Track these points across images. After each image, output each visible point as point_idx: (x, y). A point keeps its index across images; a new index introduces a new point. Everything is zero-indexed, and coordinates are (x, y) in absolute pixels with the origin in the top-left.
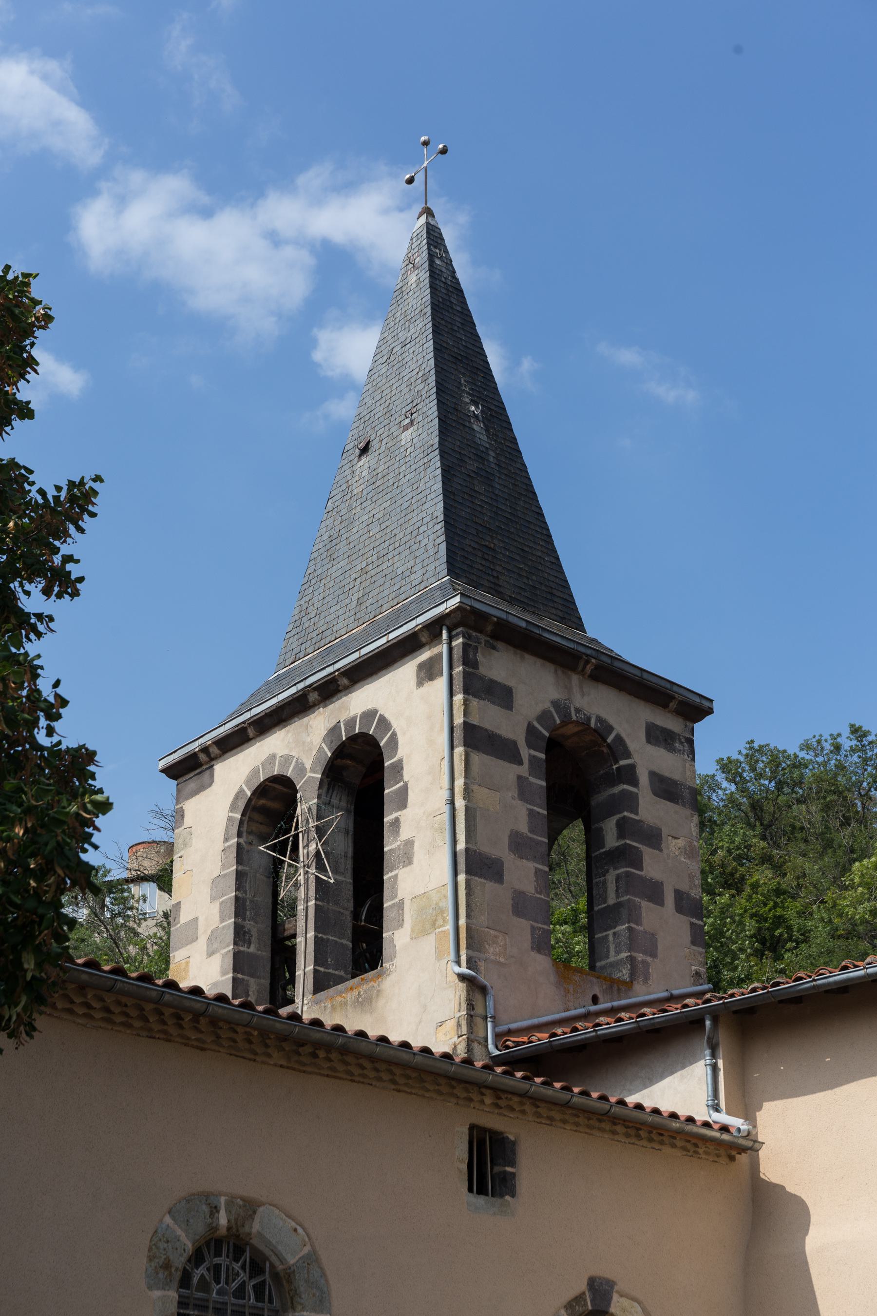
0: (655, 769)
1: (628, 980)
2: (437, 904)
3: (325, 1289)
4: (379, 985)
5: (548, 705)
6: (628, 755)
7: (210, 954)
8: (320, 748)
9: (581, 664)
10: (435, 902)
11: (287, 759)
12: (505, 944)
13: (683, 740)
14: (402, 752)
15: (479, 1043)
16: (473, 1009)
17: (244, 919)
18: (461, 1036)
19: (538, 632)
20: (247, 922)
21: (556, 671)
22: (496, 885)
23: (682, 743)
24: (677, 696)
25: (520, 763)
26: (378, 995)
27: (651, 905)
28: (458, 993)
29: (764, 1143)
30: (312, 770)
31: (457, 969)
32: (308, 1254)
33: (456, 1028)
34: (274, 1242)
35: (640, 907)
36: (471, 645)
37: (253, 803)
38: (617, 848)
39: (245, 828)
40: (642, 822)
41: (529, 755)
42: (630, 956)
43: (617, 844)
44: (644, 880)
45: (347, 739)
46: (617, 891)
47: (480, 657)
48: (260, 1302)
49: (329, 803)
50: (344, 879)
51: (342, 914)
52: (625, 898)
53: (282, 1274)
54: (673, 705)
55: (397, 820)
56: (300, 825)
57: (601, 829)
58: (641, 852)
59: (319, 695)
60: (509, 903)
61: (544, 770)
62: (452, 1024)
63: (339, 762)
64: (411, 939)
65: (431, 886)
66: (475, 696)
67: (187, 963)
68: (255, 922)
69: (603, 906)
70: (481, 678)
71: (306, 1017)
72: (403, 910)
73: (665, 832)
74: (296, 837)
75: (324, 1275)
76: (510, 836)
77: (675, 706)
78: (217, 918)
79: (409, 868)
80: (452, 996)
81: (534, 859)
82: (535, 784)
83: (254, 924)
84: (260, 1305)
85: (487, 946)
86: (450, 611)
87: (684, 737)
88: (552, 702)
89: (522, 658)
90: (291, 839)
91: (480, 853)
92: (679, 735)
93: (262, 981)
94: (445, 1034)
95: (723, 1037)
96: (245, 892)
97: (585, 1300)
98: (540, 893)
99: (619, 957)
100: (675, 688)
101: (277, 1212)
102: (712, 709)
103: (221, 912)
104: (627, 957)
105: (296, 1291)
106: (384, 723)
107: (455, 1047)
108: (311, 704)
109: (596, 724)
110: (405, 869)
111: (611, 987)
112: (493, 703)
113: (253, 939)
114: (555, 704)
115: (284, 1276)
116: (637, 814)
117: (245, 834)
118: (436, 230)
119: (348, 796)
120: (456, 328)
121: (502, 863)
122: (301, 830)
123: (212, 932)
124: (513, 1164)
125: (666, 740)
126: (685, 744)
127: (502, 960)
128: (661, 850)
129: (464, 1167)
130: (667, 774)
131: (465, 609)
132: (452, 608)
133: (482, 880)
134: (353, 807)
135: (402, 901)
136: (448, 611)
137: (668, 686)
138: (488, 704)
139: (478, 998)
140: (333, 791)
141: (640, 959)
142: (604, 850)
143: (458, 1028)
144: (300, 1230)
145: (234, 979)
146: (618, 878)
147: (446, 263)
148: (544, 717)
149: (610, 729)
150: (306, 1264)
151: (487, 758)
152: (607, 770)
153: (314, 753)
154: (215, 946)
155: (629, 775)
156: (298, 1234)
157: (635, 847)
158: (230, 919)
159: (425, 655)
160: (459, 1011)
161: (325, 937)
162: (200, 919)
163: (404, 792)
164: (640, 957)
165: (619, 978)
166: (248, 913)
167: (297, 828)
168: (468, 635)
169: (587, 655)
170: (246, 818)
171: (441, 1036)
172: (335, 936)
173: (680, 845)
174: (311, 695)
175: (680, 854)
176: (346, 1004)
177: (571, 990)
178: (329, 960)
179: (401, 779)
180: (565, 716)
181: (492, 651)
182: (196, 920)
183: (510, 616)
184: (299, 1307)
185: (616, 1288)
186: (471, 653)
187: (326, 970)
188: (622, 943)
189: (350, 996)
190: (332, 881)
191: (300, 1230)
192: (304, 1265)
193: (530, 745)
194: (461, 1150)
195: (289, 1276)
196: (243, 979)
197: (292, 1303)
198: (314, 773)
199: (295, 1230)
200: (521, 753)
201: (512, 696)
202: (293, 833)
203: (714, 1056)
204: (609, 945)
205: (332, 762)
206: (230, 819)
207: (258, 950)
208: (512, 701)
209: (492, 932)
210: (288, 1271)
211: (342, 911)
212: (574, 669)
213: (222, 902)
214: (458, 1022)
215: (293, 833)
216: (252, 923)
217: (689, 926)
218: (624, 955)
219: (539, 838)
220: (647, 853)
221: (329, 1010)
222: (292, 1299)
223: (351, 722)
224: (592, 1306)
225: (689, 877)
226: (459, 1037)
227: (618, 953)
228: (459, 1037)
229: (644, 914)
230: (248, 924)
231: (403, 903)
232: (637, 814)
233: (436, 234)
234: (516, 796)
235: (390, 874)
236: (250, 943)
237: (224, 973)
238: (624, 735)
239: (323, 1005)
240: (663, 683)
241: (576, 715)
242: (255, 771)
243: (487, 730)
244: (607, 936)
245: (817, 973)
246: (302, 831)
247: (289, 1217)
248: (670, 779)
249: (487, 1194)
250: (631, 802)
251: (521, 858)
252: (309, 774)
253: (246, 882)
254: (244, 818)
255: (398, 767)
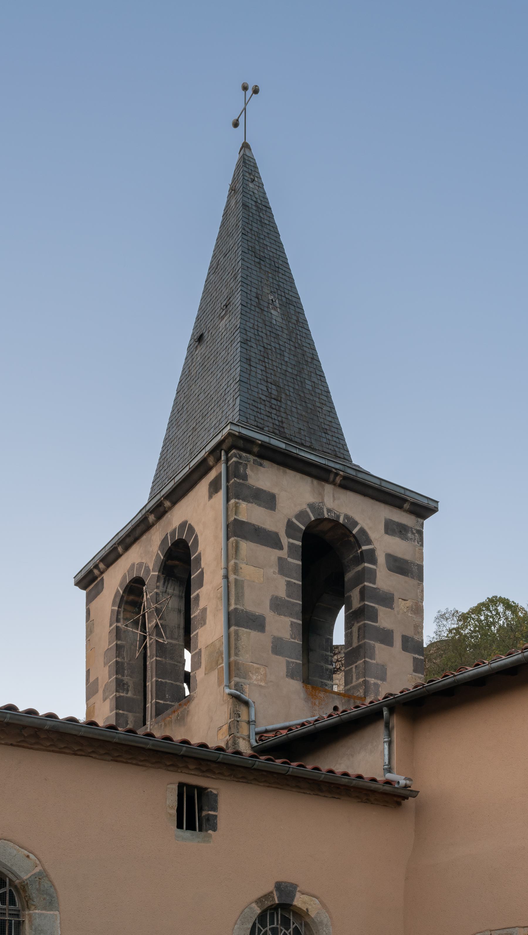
0: (390, 551)
1: (363, 696)
2: (219, 649)
3: (55, 895)
4: (188, 707)
5: (304, 507)
6: (369, 541)
7: (104, 700)
8: (158, 554)
9: (332, 477)
10: (217, 648)
11: (141, 565)
12: (265, 673)
13: (414, 532)
14: (201, 548)
15: (244, 739)
16: (239, 717)
17: (123, 676)
18: (231, 735)
19: (295, 452)
20: (125, 677)
21: (312, 482)
22: (259, 634)
23: (413, 533)
24: (409, 499)
25: (281, 548)
26: (187, 714)
27: (383, 646)
28: (229, 707)
29: (419, 792)
30: (154, 570)
31: (227, 691)
32: (39, 872)
33: (228, 730)
34: (9, 865)
35: (374, 647)
36: (242, 463)
37: (125, 598)
38: (360, 608)
39: (121, 616)
40: (379, 589)
41: (289, 543)
42: (364, 680)
43: (359, 606)
44: (378, 629)
45: (172, 545)
46: (358, 637)
47: (249, 471)
48: (3, 905)
49: (166, 592)
50: (177, 643)
51: (177, 665)
52: (363, 642)
53: (19, 887)
54: (406, 506)
55: (198, 595)
56: (146, 608)
57: (350, 596)
58: (377, 610)
59: (155, 517)
60: (269, 646)
61: (300, 553)
62: (226, 728)
63: (170, 562)
64: (205, 674)
65: (215, 638)
66: (244, 500)
67: (94, 707)
68: (131, 677)
69: (350, 648)
70: (249, 487)
71: (158, 734)
72: (201, 656)
73: (396, 597)
74: (144, 615)
75: (53, 885)
76: (271, 600)
77: (408, 507)
78: (107, 676)
79: (204, 627)
80: (226, 710)
81: (291, 615)
82: (293, 563)
83: (131, 679)
84: (4, 907)
85: (251, 675)
86: (224, 437)
87: (415, 529)
88: (308, 505)
89: (285, 472)
90: (141, 617)
91: (246, 612)
92: (411, 528)
93: (138, 715)
94: (222, 734)
95: (395, 721)
96: (124, 658)
97: (273, 897)
98: (294, 639)
99: (358, 682)
100: (408, 493)
101: (12, 844)
102: (437, 508)
103: (109, 671)
104: (363, 681)
105: (30, 897)
106: (191, 529)
107: (228, 742)
108: (151, 524)
109: (344, 520)
110: (202, 628)
111: (349, 701)
112: (260, 505)
113: (130, 688)
114: (311, 506)
115: (21, 887)
116: (374, 583)
117: (122, 620)
118: (251, 160)
119: (180, 586)
120: (262, 237)
121: (264, 619)
122: (146, 611)
123: (105, 685)
124: (215, 809)
125: (400, 531)
126: (416, 534)
127: (263, 684)
128: (392, 609)
129: (174, 812)
130: (400, 555)
131: (234, 435)
132: (225, 435)
133: (248, 630)
134: (184, 594)
135: (200, 650)
136: (223, 437)
137: (402, 491)
138: (255, 506)
139: (243, 710)
140: (168, 584)
141: (372, 682)
142: (352, 611)
143: (229, 730)
144: (31, 856)
145: (117, 714)
146: (359, 629)
147: (259, 187)
148: (301, 515)
149: (356, 524)
150: (37, 879)
151: (252, 545)
152: (354, 554)
153: (154, 558)
154: (107, 694)
155: (371, 556)
156: (31, 859)
157: (372, 606)
158: (114, 676)
159: (212, 475)
160: (230, 719)
161: (163, 681)
162: (99, 678)
163: (201, 575)
164: (372, 681)
165: (358, 695)
166: (126, 672)
167: (144, 610)
168: (239, 455)
169: (336, 469)
170: (122, 610)
171: (220, 737)
172: (171, 680)
173: (407, 605)
174: (150, 517)
175: (407, 611)
176: (171, 721)
177: (317, 703)
178: (167, 695)
179: (200, 567)
180: (319, 515)
181: (259, 467)
182: (97, 679)
183: (272, 440)
184: (33, 907)
185: (298, 889)
186: (242, 469)
187: (165, 702)
188: (361, 672)
189: (174, 716)
190: (166, 643)
191: (31, 856)
192: (36, 879)
193: (289, 535)
194: (172, 799)
195: (24, 887)
196: (124, 714)
197: (27, 905)
198: (154, 572)
199: (28, 856)
200: (282, 541)
201: (275, 500)
202: (142, 613)
203: (390, 735)
204: (352, 675)
205: (165, 563)
206: (112, 611)
207: (134, 695)
208: (275, 504)
209: (255, 665)
210: (23, 884)
211: (176, 663)
212: (327, 481)
213: (110, 665)
214: (230, 725)
215: (142, 613)
216: (129, 678)
217: (412, 660)
218: (361, 680)
219: (295, 601)
220: (382, 611)
221: (163, 727)
222: (27, 902)
223: (173, 533)
224: (278, 900)
225: (414, 627)
226: (229, 736)
227: (358, 679)
228: (229, 736)
229: (377, 652)
230: (126, 679)
231: (201, 652)
232: (374, 583)
233: (252, 164)
234: (277, 571)
235: (195, 633)
236: (128, 691)
237: (111, 711)
238: (366, 528)
239: (160, 724)
240: (398, 489)
241: (328, 514)
242: (124, 577)
243: (254, 525)
244: (352, 668)
245: (458, 670)
246: (147, 612)
247: (22, 848)
248: (403, 559)
249: (194, 829)
250: (372, 576)
251: (280, 614)
252: (152, 573)
253: (124, 652)
254: (120, 609)
255: (199, 559)
